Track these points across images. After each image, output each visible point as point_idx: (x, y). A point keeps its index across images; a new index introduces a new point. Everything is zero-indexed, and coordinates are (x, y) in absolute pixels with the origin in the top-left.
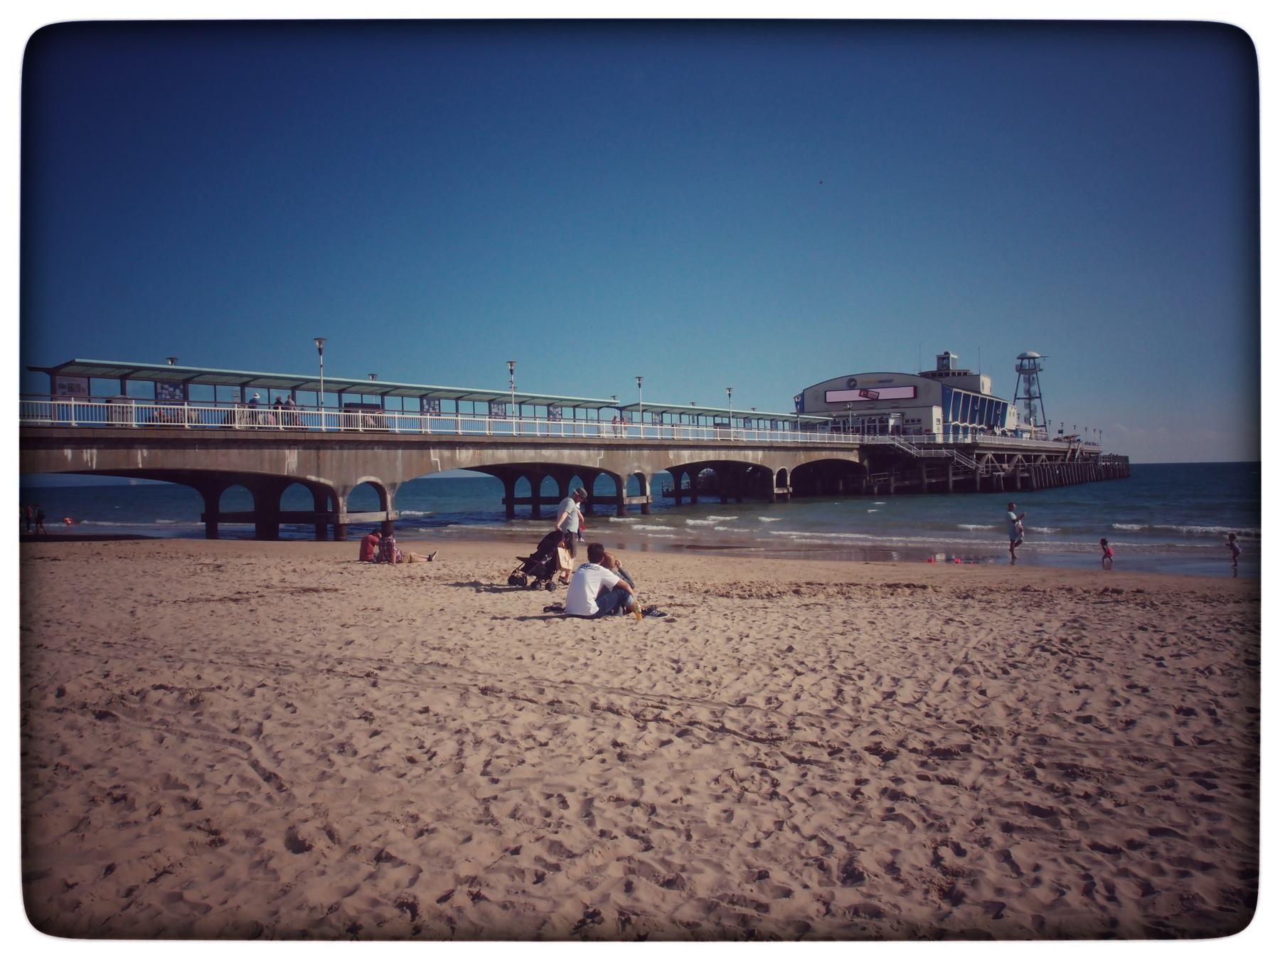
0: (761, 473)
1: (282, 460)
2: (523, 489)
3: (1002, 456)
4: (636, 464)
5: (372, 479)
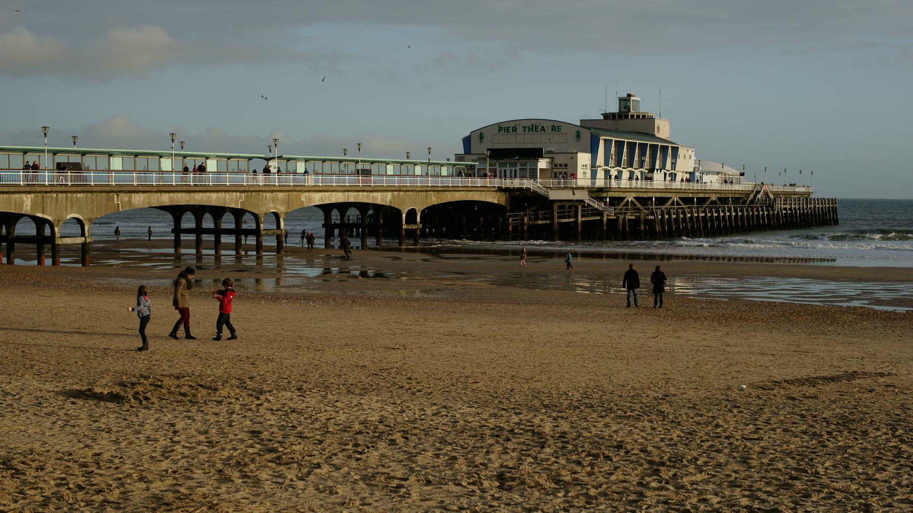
0: (391, 213)
1: (22, 203)
2: (188, 222)
3: (570, 207)
4: (272, 205)
5: (76, 216)
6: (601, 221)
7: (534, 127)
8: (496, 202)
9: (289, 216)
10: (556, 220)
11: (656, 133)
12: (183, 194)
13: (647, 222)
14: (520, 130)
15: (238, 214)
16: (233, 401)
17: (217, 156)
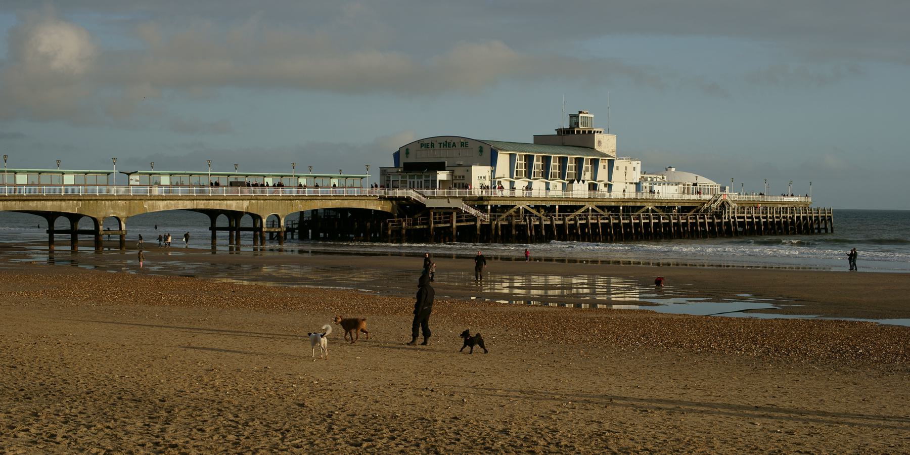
6: (475, 226)
7: (426, 144)
8: (379, 209)
9: (130, 221)
10: (432, 225)
11: (596, 147)
12: (18, 202)
13: (518, 227)
14: (437, 146)
15: (74, 218)
16: (717, 443)
17: (28, 172)
